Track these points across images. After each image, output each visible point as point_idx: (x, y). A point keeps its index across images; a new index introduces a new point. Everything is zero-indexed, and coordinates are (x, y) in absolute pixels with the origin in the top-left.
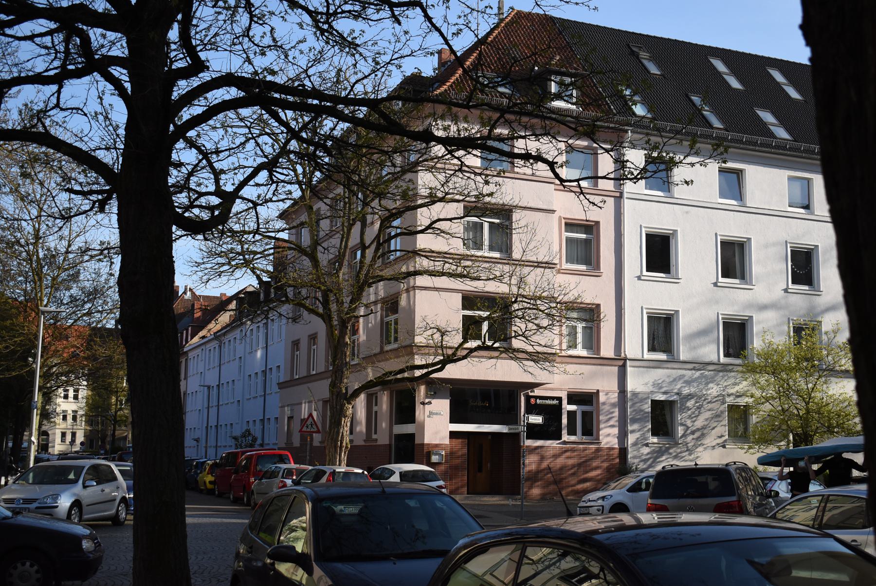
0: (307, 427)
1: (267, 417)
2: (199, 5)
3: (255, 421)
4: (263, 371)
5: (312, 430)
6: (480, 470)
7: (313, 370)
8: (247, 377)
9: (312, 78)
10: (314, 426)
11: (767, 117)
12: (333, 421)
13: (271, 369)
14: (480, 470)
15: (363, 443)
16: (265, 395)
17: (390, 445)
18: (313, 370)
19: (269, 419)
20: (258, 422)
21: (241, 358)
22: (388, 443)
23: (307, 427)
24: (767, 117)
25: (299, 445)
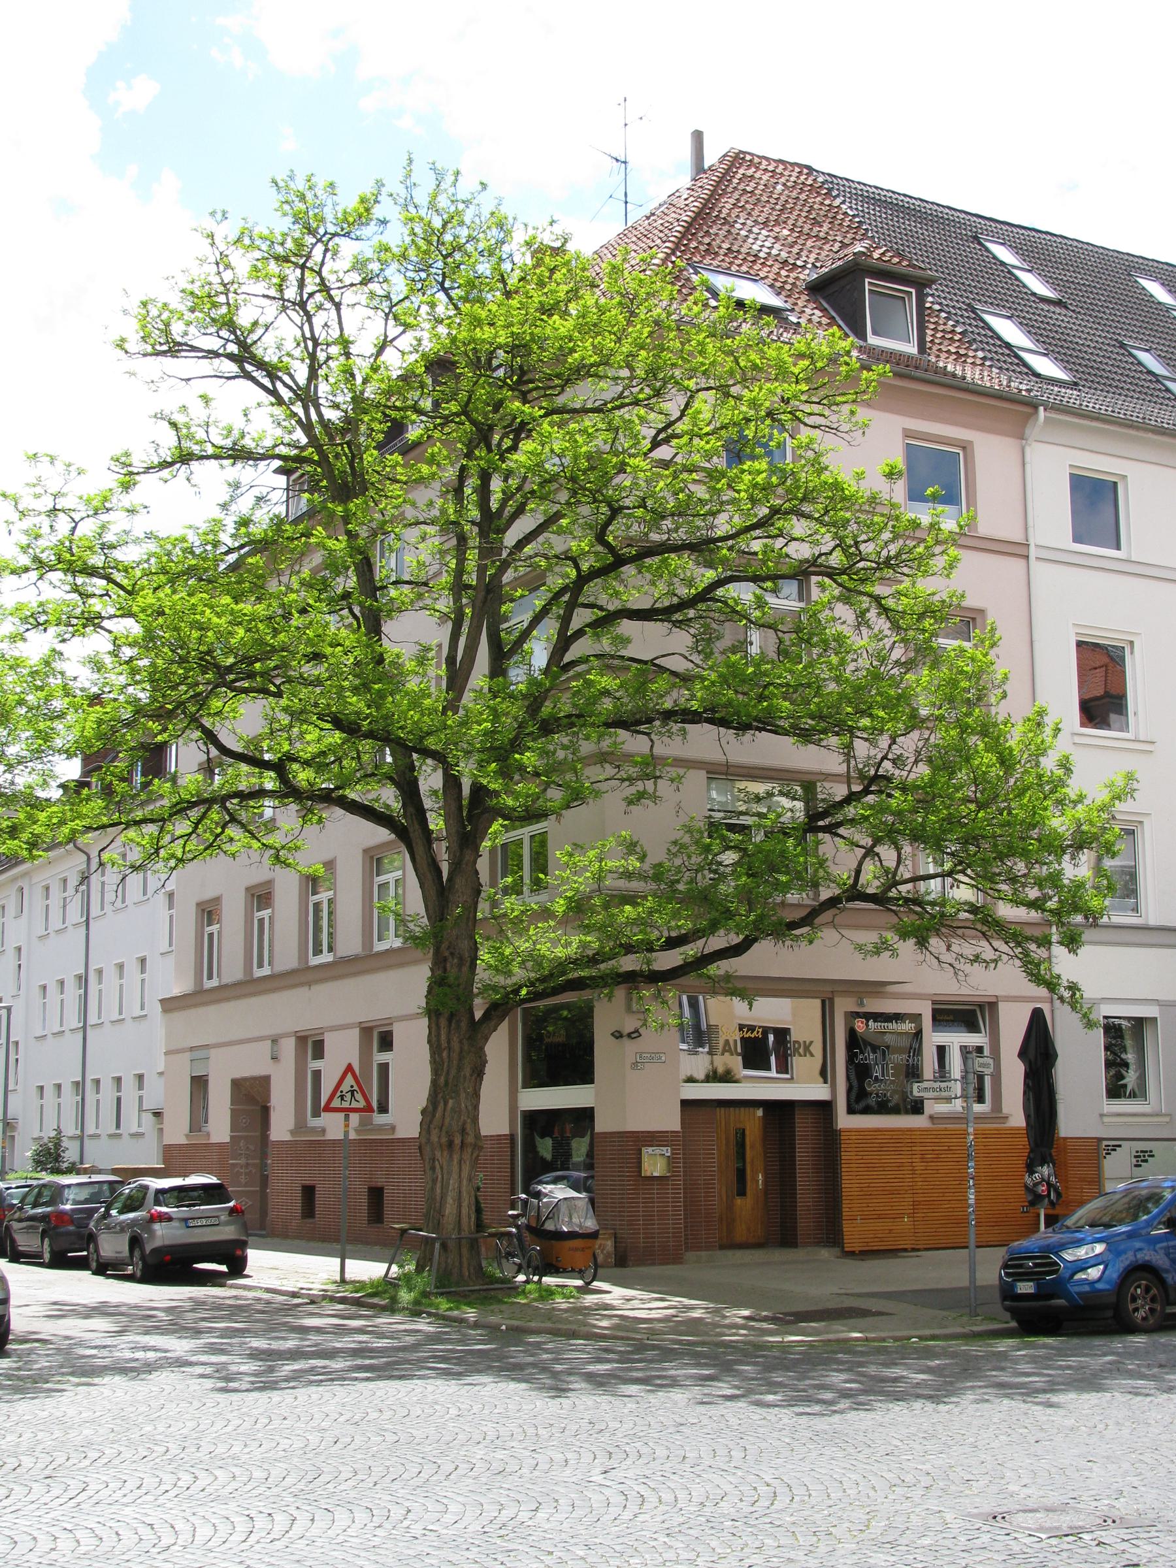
0: (342, 1097)
1: (90, 1076)
2: (859, 729)
3: (59, 1086)
4: (79, 977)
5: (354, 1105)
6: (742, 1192)
7: (210, 977)
8: (37, 992)
9: (894, 747)
10: (358, 1096)
11: (1036, 284)
12: (442, 1080)
13: (100, 972)
14: (742, 1192)
15: (183, 1141)
16: (84, 1028)
17: (512, 1137)
18: (210, 977)
19: (97, 1082)
20: (67, 1089)
21: (19, 949)
22: (506, 1131)
23: (342, 1097)
24: (1036, 284)
25: (227, 1140)
